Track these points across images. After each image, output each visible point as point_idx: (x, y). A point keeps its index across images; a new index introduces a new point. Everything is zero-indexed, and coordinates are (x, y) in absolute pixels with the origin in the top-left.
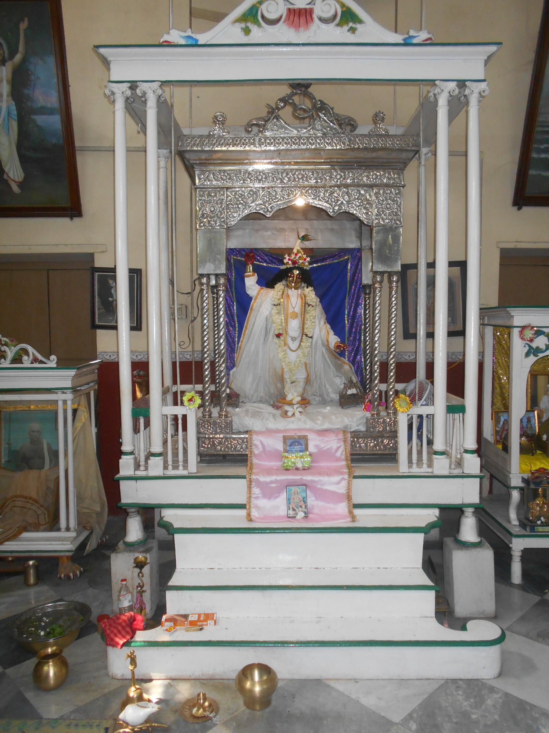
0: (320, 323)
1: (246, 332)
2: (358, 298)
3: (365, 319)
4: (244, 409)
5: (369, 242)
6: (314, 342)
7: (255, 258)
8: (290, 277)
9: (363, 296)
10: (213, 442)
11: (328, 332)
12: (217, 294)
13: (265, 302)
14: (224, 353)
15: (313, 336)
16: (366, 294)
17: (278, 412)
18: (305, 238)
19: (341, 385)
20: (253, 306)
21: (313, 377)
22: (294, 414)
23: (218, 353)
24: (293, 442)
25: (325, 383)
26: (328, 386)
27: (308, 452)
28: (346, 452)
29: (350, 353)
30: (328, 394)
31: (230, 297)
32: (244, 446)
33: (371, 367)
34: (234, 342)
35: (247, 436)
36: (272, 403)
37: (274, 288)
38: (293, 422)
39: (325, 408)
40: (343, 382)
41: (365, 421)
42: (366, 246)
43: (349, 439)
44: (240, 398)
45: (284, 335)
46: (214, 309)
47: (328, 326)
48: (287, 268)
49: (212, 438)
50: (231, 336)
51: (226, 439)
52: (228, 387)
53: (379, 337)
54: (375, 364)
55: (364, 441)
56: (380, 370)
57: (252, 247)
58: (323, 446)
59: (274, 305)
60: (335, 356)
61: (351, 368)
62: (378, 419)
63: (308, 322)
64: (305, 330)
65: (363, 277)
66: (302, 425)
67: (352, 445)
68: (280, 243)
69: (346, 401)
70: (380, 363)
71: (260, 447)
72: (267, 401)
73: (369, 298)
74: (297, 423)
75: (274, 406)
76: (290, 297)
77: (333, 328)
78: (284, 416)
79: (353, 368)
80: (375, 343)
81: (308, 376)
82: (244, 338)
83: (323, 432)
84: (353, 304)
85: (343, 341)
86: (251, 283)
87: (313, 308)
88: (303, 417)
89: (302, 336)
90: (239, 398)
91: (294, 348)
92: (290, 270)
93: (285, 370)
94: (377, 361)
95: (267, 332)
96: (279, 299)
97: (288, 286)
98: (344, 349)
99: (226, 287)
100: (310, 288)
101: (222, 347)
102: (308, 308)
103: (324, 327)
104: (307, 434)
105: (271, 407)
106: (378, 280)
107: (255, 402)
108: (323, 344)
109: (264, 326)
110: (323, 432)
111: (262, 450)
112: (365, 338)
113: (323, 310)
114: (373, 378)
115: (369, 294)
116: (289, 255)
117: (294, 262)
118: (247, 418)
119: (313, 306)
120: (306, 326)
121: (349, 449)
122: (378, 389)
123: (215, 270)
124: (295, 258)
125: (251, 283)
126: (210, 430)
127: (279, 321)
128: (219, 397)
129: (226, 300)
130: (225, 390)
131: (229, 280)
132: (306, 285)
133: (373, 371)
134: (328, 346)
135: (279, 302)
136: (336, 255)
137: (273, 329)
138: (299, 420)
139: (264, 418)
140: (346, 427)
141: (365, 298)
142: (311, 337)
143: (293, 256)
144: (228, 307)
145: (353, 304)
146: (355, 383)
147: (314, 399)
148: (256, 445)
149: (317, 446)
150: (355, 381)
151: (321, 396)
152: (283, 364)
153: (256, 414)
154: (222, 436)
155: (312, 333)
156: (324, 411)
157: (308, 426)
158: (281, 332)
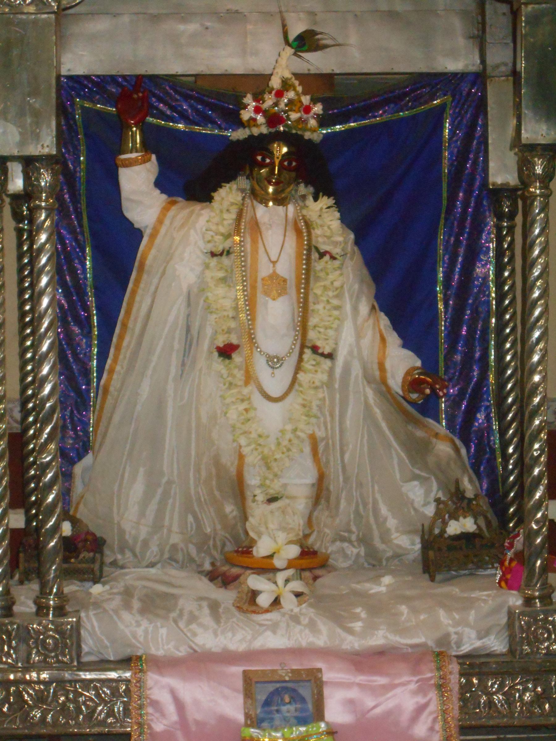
0: (355, 309)
1: (126, 341)
2: (478, 228)
3: (501, 297)
4: (120, 586)
5: (510, 53)
6: (338, 371)
7: (152, 107)
8: (262, 165)
9: (491, 222)
10: (19, 695)
11: (383, 340)
12: (31, 221)
13: (183, 245)
14: (53, 409)
15: (335, 350)
16: (500, 216)
17: (227, 597)
18: (306, 42)
19: (426, 504)
20: (144, 258)
21: (335, 481)
22: (276, 602)
23: (34, 409)
24: (277, 692)
25: (375, 503)
26: (384, 510)
27: (323, 725)
28: (445, 721)
29: (455, 403)
30: (385, 537)
31: (72, 231)
32: (118, 708)
33: (522, 448)
34: (86, 372)
35: (128, 675)
36: (207, 567)
37: (209, 199)
38: (274, 627)
39: (376, 579)
40: (433, 495)
41: (504, 620)
42: (497, 66)
43: (455, 680)
44: (107, 552)
45: (245, 349)
46: (21, 269)
47: (384, 321)
48: (251, 137)
49: (16, 682)
50: (75, 355)
51: (61, 682)
52: (66, 516)
53: (545, 354)
54: (535, 437)
55: (502, 686)
56: (549, 458)
57: (141, 70)
58: (370, 702)
59: (213, 254)
60: (405, 412)
61: (457, 450)
62: (547, 614)
63: (320, 307)
64: (312, 335)
65: (491, 164)
66: (302, 637)
67: (462, 699)
68: (225, 58)
69: (442, 558)
70: (550, 434)
71: (171, 708)
72: (192, 560)
73: (511, 229)
74: (285, 632)
75: (213, 576)
76: (263, 228)
77: (398, 325)
78: (245, 607)
79: (463, 451)
80: (532, 372)
81: (321, 478)
82: (120, 362)
83: (368, 661)
84: (462, 251)
85: (429, 366)
86: (138, 184)
87: (337, 263)
88: (307, 611)
89: (301, 353)
90: (102, 553)
91: (275, 390)
92: (261, 144)
93: (249, 459)
94: (540, 429)
95: (190, 340)
96: (228, 236)
97: (254, 194)
98: (433, 390)
99: (59, 198)
100: (325, 201)
101: (47, 389)
102: (319, 265)
103: (371, 322)
104: (319, 665)
105: (205, 580)
106: (539, 170)
107: (152, 565)
108: (368, 379)
109: (182, 322)
110: (368, 661)
111: (174, 717)
112: (500, 357)
113: (365, 271)
114: (528, 482)
115: (512, 216)
116: (258, 97)
117: (273, 119)
118: (126, 616)
119: (333, 258)
120: (313, 321)
121: (456, 712)
122: (544, 516)
123: (22, 144)
124: (276, 104)
125: (138, 184)
126: (8, 655)
127: (228, 303)
128: (38, 548)
129: (61, 239)
130: (57, 527)
131: (69, 178)
132: (311, 189)
133: (527, 460)
134: (384, 381)
135: (227, 244)
136: (406, 94)
137: (209, 331)
138: (295, 619)
139: (181, 615)
140: (444, 640)
141: (499, 229)
142: (330, 356)
143: (269, 101)
144: (65, 264)
145: (462, 251)
146: (470, 500)
147: (342, 551)
148: (155, 704)
149: (351, 703)
150: (470, 494)
151: (365, 540)
152: (243, 441)
153: (156, 604)
154: (45, 676)
155: (331, 342)
156: (375, 589)
157: (321, 641)
158: (235, 341)
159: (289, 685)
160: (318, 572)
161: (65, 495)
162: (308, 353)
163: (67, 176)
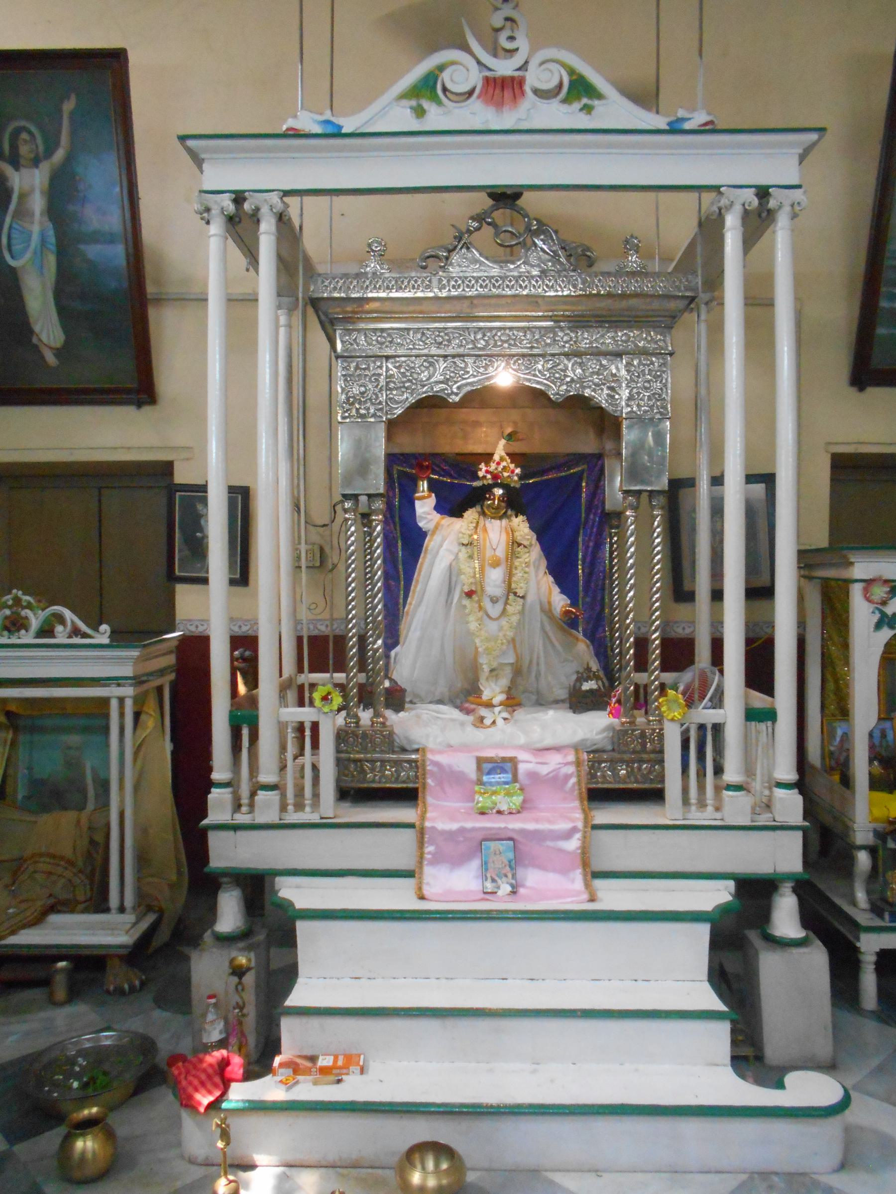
8: (489, 499)
22: (494, 722)
47: (551, 579)
78: (478, 725)
86: (425, 508)
92: (488, 489)
100: (521, 518)
117: (495, 477)
124: (496, 469)
125: (425, 508)
134: (550, 610)
142: (523, 597)
143: (493, 466)
144: (389, 545)
150: (594, 669)
158: (474, 589)
159: (500, 765)
160: (515, 708)
161: (387, 665)
162: (511, 597)
163: (390, 506)
